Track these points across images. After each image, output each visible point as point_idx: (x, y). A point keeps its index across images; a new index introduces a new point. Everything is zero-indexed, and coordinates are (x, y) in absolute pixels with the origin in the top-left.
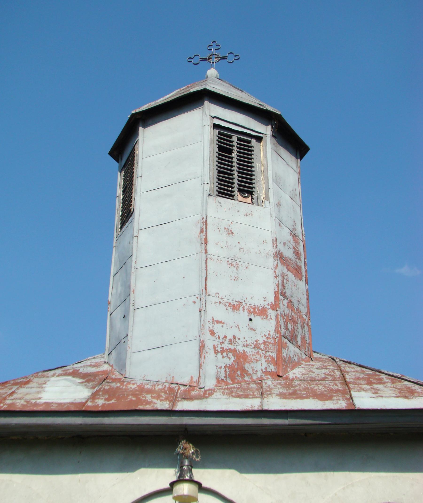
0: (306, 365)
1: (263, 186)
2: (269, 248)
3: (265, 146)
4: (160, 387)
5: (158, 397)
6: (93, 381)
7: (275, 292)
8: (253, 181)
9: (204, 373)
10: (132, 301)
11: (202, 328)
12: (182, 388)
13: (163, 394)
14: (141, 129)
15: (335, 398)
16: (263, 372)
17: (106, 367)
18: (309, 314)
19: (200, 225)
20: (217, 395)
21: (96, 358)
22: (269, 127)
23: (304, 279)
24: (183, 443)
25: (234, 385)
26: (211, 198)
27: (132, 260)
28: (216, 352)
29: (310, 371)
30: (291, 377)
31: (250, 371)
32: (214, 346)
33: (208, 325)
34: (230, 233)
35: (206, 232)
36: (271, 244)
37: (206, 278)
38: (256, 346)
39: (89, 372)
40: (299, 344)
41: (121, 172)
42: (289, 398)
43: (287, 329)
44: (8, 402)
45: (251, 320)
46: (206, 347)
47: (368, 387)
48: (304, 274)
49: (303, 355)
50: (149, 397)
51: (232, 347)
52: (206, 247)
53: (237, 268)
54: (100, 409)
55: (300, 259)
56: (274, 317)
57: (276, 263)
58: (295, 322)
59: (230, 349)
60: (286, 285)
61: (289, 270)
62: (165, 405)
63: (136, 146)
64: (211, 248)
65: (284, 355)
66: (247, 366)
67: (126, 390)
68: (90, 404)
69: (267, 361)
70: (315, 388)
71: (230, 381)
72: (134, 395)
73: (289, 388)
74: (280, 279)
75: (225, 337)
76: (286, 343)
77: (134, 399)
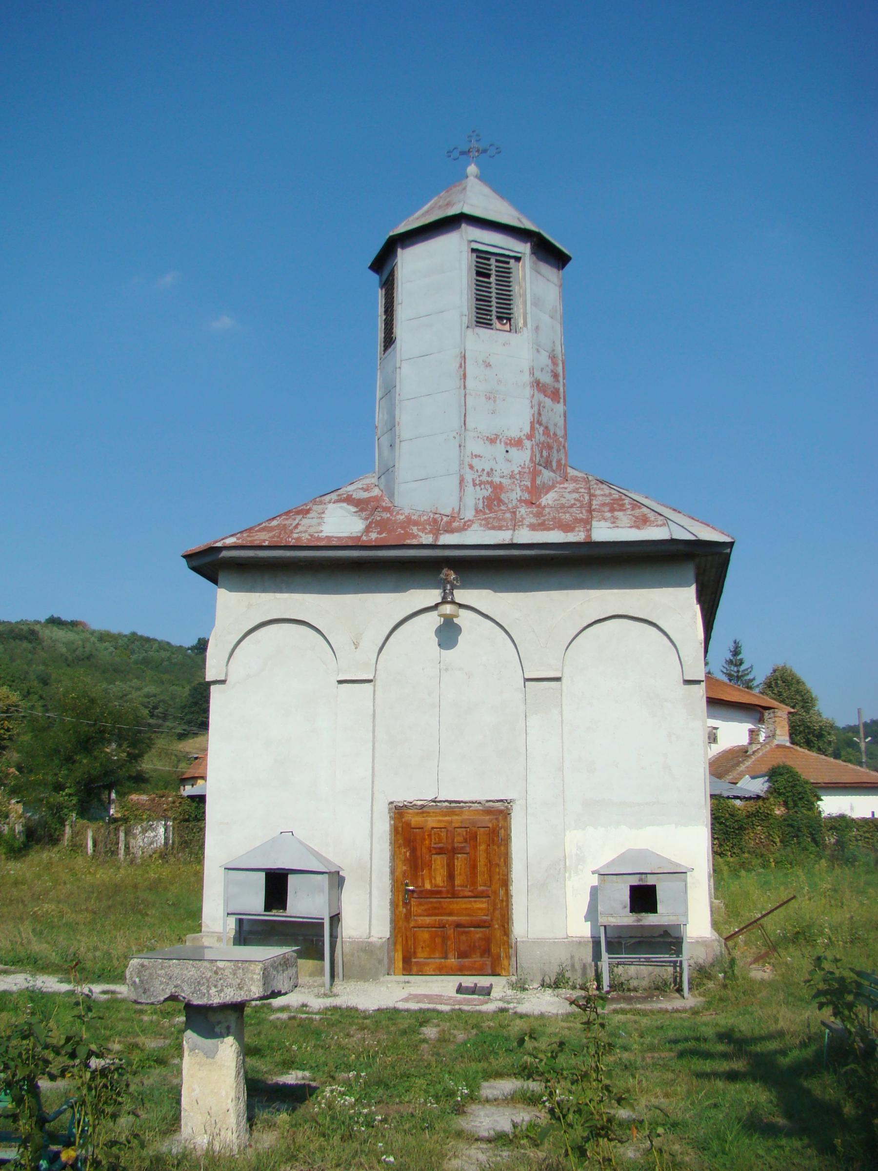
0: (560, 488)
1: (521, 311)
2: (526, 378)
3: (524, 267)
4: (425, 518)
5: (423, 530)
6: (366, 510)
7: (531, 422)
8: (511, 307)
9: (464, 506)
10: (397, 433)
11: (461, 463)
12: (445, 519)
13: (427, 527)
14: (399, 250)
15: (577, 529)
16: (518, 501)
17: (376, 492)
18: (565, 436)
19: (459, 359)
20: (475, 526)
21: (367, 477)
22: (528, 245)
23: (562, 400)
24: (445, 571)
25: (491, 515)
26: (470, 331)
27: (395, 392)
28: (475, 485)
29: (562, 496)
30: (543, 504)
31: (506, 501)
32: (473, 479)
33: (467, 460)
34: (488, 365)
35: (465, 367)
36: (528, 373)
37: (465, 414)
38: (512, 476)
39: (362, 497)
40: (554, 468)
41: (382, 289)
42: (537, 530)
43: (542, 456)
44: (295, 536)
45: (507, 451)
46: (465, 481)
47: (608, 515)
48: (562, 396)
49: (558, 477)
50: (415, 530)
51: (489, 479)
52: (464, 382)
53: (495, 401)
54: (374, 544)
55: (558, 381)
56: (529, 447)
57: (532, 393)
58: (550, 448)
59: (487, 481)
60: (542, 413)
61: (546, 396)
62: (428, 539)
63: (395, 268)
64: (470, 383)
65: (538, 482)
66: (503, 496)
67: (396, 520)
68: (364, 538)
69: (522, 490)
70: (563, 517)
71: (487, 511)
72: (403, 528)
73: (540, 518)
74: (536, 408)
75: (483, 470)
76: (541, 471)
77: (402, 532)
